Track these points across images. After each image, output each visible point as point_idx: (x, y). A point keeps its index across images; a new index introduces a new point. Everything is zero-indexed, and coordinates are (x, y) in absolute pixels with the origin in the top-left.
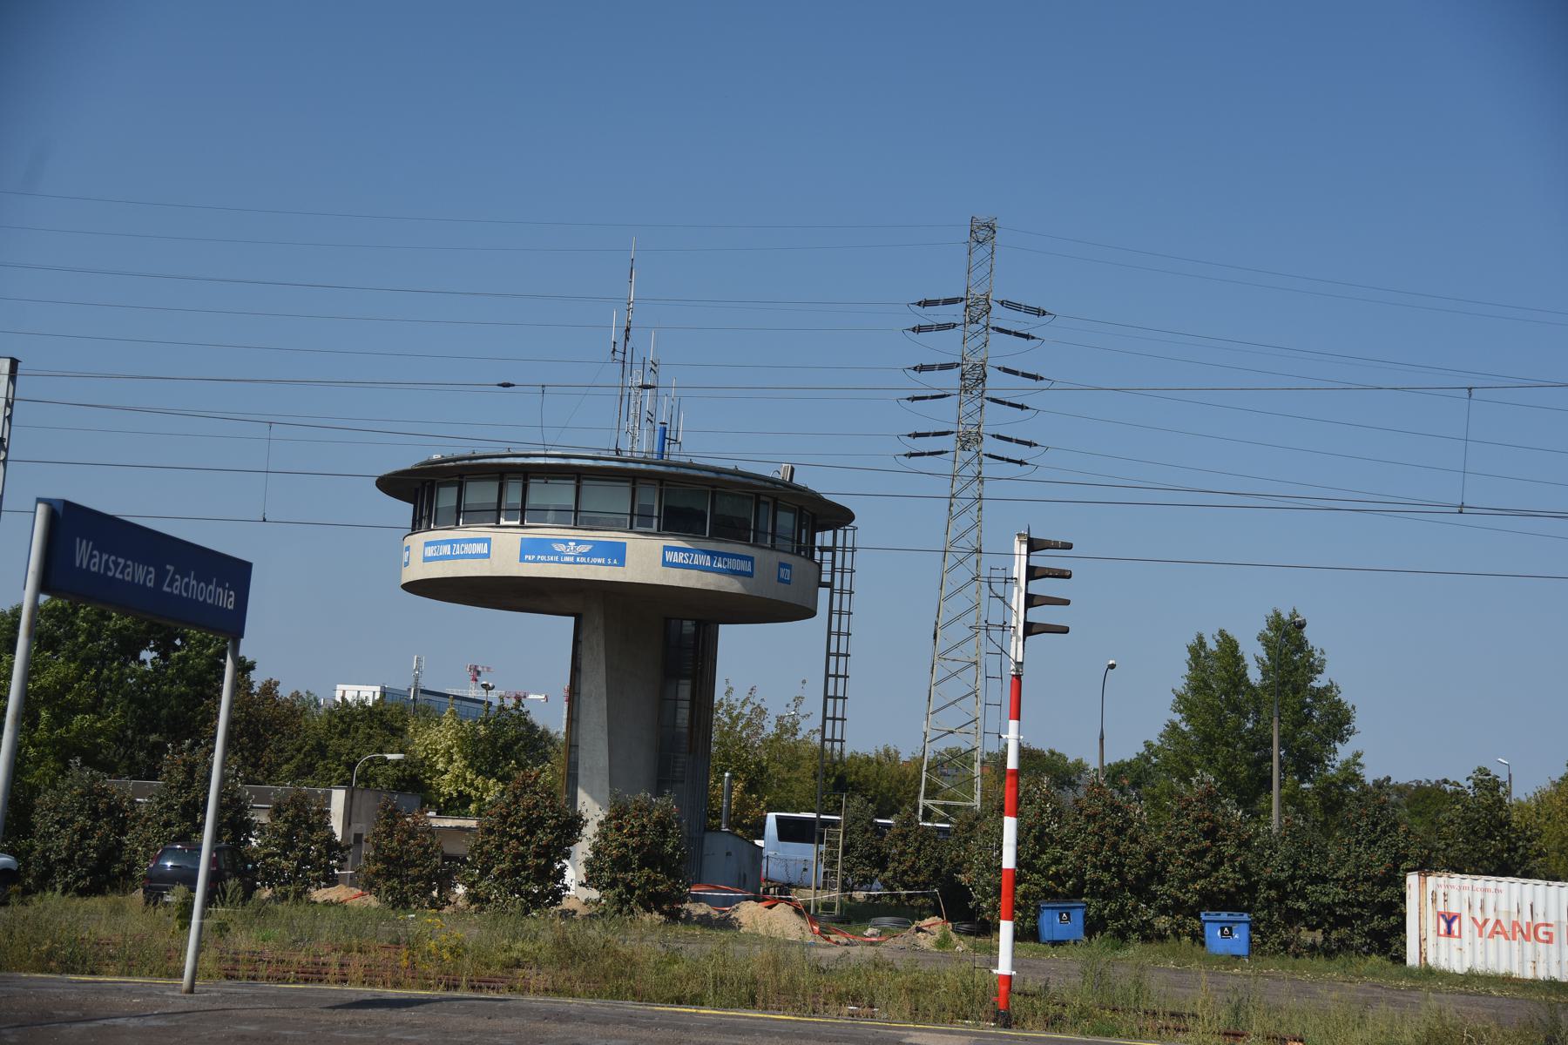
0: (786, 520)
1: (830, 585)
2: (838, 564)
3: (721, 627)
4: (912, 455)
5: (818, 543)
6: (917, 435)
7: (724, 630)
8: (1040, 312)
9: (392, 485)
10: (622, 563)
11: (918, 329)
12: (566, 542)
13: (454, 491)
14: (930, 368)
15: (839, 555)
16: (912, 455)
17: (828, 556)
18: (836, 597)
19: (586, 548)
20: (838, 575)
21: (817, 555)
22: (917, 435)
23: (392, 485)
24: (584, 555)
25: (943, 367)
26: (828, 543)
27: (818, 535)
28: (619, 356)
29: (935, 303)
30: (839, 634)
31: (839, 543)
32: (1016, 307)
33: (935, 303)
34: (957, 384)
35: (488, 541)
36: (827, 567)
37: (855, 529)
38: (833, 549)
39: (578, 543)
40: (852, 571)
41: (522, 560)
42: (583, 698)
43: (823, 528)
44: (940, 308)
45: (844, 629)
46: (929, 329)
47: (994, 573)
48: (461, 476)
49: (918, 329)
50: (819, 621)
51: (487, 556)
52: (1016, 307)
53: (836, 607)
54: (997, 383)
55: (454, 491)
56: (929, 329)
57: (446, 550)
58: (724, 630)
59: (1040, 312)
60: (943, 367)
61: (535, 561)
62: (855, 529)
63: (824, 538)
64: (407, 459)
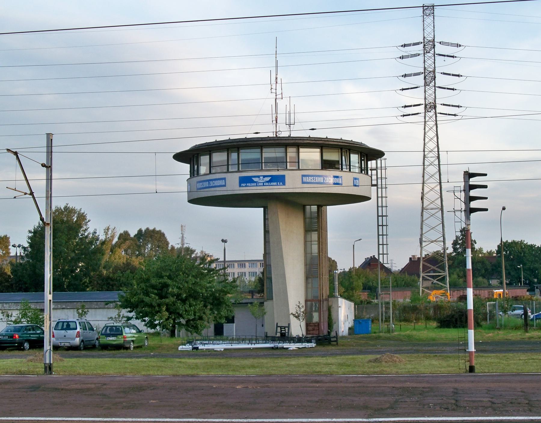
0: (355, 158)
1: (376, 185)
2: (379, 176)
3: (328, 207)
4: (404, 116)
5: (369, 166)
6: (406, 107)
7: (263, 209)
8: (458, 46)
9: (180, 157)
10: (284, 184)
11: (402, 58)
12: (258, 177)
13: (208, 157)
14: (410, 75)
15: (379, 171)
16: (404, 116)
17: (374, 172)
18: (380, 190)
19: (268, 179)
20: (379, 181)
21: (369, 172)
22: (406, 107)
23: (180, 157)
24: (267, 182)
25: (415, 74)
26: (374, 166)
27: (369, 162)
28: (274, 91)
29: (409, 45)
30: (382, 207)
31: (379, 165)
32: (447, 44)
33: (409, 45)
34: (422, 83)
35: (225, 179)
36: (374, 177)
37: (385, 159)
38: (376, 169)
39: (264, 176)
40: (386, 178)
41: (240, 186)
42: (271, 244)
43: (371, 160)
44: (412, 47)
45: (384, 205)
46: (407, 57)
47: (456, 189)
48: (210, 151)
49: (402, 58)
50: (373, 202)
51: (225, 186)
52: (447, 44)
53: (380, 195)
54: (441, 80)
55: (208, 157)
56: (407, 57)
57: (206, 184)
58: (263, 209)
59: (458, 46)
60: (415, 74)
61: (246, 186)
62: (385, 159)
63: (372, 164)
64: (186, 146)
